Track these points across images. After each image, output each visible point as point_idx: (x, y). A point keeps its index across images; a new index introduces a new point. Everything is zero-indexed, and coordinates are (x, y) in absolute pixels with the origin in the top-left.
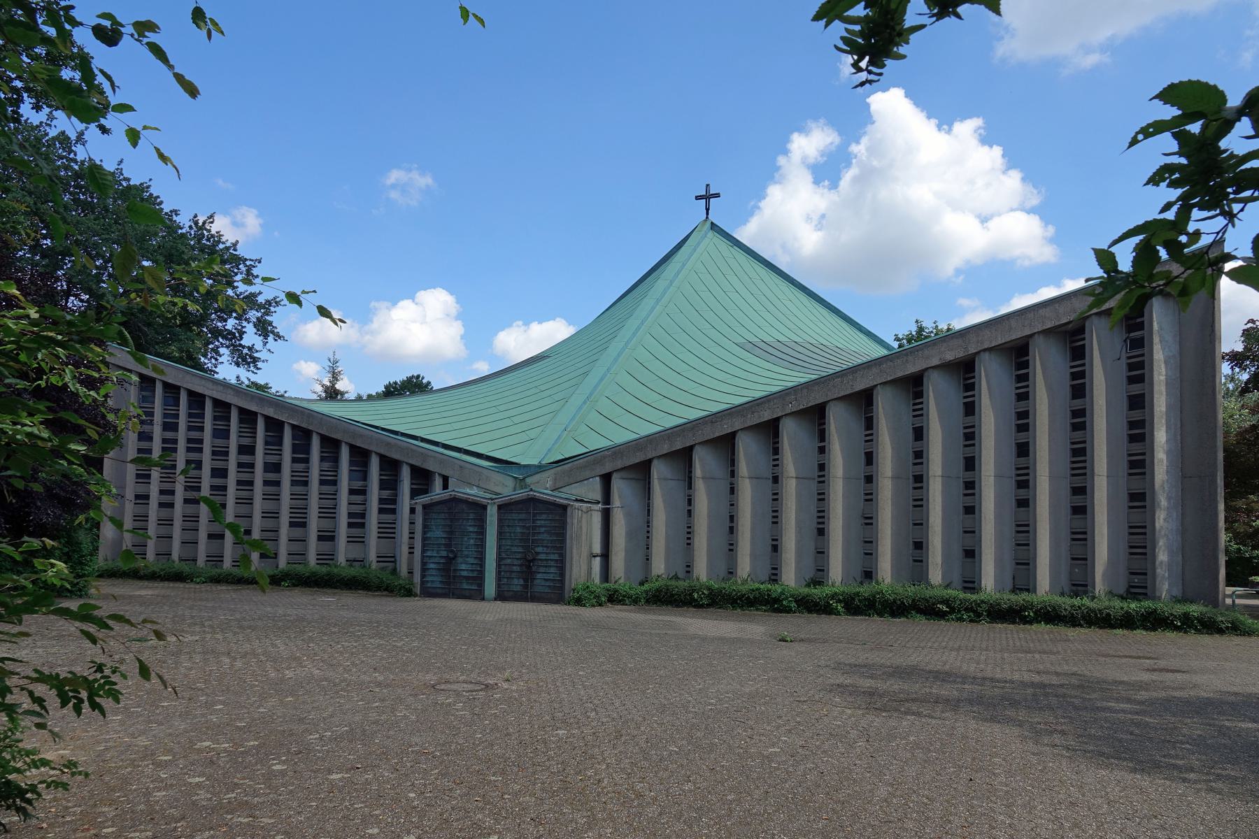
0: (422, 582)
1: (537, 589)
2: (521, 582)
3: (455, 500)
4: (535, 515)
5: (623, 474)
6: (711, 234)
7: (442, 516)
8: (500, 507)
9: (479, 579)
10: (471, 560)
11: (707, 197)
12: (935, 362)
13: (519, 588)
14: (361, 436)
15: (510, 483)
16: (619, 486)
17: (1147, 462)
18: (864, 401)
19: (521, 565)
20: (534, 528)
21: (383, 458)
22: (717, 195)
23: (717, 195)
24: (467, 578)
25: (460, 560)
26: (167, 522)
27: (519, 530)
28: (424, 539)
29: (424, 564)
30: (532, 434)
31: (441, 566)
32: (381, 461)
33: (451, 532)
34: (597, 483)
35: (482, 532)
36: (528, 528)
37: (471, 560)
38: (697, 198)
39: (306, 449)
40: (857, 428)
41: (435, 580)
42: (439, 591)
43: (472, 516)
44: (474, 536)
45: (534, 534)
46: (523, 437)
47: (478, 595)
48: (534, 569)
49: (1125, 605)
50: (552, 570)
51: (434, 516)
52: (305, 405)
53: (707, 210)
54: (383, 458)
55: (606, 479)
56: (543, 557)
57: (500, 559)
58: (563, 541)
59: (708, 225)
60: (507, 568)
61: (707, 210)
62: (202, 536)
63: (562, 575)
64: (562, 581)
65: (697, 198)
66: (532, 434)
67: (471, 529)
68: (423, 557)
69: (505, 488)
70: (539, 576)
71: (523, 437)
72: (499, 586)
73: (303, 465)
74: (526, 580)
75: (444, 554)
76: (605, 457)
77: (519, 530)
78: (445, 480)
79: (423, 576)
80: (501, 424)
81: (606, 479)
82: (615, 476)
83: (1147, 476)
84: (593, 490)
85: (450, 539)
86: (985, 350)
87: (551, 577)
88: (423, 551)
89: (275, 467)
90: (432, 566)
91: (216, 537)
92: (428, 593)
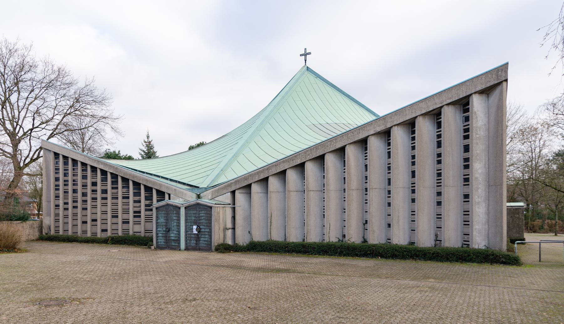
0: (157, 242)
3: (168, 205)
6: (307, 72)
7: (163, 212)
8: (186, 208)
9: (178, 241)
12: (372, 132)
13: (194, 245)
14: (136, 177)
15: (194, 196)
16: (240, 196)
17: (470, 179)
18: (363, 143)
20: (199, 217)
21: (146, 187)
22: (310, 53)
23: (310, 53)
24: (174, 240)
25: (171, 232)
26: (66, 217)
27: (193, 218)
28: (157, 223)
29: (157, 234)
30: (208, 173)
31: (164, 235)
33: (167, 220)
34: (229, 195)
35: (179, 219)
36: (197, 217)
37: (175, 232)
38: (301, 55)
39: (117, 182)
40: (360, 155)
41: (162, 241)
42: (164, 246)
43: (175, 212)
44: (176, 221)
47: (178, 248)
50: (207, 236)
51: (160, 212)
53: (306, 61)
54: (146, 187)
55: (233, 193)
58: (211, 223)
59: (306, 68)
61: (306, 61)
62: (79, 222)
63: (211, 239)
64: (211, 241)
65: (301, 55)
67: (175, 218)
68: (157, 231)
69: (191, 198)
70: (202, 239)
71: (205, 174)
72: (186, 244)
74: (196, 241)
75: (164, 229)
76: (232, 183)
77: (193, 218)
78: (169, 195)
79: (157, 240)
80: (196, 169)
81: (233, 193)
82: (236, 192)
83: (470, 186)
84: (227, 198)
86: (395, 125)
87: (206, 239)
88: (157, 228)
89: (105, 192)
90: (160, 235)
91: (85, 222)
92: (159, 248)
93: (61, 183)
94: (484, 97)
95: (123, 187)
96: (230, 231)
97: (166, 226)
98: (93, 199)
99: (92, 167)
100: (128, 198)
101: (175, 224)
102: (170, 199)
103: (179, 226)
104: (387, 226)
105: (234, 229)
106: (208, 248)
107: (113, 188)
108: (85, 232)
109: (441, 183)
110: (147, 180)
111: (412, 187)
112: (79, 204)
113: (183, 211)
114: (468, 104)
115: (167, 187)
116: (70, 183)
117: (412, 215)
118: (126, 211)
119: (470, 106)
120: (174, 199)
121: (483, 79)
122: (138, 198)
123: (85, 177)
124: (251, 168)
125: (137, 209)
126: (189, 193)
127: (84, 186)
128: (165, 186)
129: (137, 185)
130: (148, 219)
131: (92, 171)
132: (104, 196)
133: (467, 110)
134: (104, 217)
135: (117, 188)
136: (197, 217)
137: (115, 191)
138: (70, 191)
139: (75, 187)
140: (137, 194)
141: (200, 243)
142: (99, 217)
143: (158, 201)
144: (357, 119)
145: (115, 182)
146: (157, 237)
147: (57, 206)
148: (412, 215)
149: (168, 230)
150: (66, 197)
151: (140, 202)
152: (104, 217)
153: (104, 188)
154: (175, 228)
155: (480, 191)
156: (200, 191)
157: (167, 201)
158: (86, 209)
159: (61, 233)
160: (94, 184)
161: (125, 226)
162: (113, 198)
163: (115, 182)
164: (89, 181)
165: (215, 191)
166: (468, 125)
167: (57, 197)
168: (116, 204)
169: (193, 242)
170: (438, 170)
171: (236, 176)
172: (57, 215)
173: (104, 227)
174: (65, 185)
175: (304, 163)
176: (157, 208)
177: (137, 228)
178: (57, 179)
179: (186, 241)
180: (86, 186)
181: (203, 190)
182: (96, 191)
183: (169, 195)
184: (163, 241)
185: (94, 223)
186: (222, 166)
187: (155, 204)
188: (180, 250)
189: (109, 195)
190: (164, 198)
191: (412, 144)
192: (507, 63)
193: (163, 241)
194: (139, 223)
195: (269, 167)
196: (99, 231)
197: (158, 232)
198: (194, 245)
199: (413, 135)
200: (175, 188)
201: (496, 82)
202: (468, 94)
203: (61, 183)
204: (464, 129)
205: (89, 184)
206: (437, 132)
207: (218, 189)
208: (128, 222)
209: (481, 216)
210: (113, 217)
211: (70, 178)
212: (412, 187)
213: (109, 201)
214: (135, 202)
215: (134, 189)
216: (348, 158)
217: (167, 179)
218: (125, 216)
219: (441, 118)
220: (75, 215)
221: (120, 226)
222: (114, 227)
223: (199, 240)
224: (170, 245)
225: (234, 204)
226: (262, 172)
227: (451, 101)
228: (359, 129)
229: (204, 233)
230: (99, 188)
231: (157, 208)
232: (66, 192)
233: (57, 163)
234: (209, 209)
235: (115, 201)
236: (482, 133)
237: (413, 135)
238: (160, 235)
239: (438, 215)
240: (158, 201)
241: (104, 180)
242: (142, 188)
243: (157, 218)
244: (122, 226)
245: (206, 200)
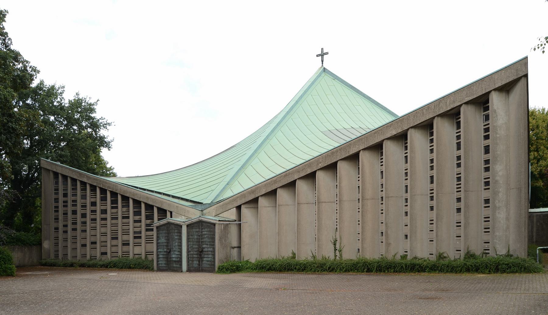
0: (158, 264)
1: (204, 265)
2: (197, 262)
3: (169, 224)
4: (202, 229)
5: (246, 206)
8: (188, 226)
9: (180, 262)
10: (177, 253)
11: (322, 55)
13: (196, 266)
19: (197, 254)
20: (202, 235)
22: (327, 53)
23: (327, 53)
25: (172, 253)
26: (66, 240)
28: (158, 243)
29: (158, 255)
30: (213, 188)
31: (165, 256)
32: (133, 202)
33: (168, 240)
35: (180, 239)
36: (199, 236)
37: (177, 253)
38: (317, 56)
41: (163, 263)
42: (165, 268)
43: (176, 231)
44: (177, 241)
45: (202, 238)
46: (209, 189)
47: (179, 270)
48: (203, 256)
49: (18, 234)
50: (210, 256)
51: (161, 232)
52: (125, 182)
53: (322, 61)
55: (239, 208)
56: (206, 250)
57: (188, 252)
60: (191, 256)
61: (322, 61)
62: (79, 245)
65: (317, 56)
66: (213, 188)
67: (176, 237)
68: (157, 252)
69: (195, 215)
70: (205, 259)
71: (209, 189)
72: (188, 265)
73: (116, 210)
74: (199, 261)
75: (165, 250)
79: (158, 261)
81: (239, 208)
84: (231, 215)
85: (168, 243)
87: (209, 259)
88: (157, 249)
89: (104, 212)
90: (161, 256)
92: (160, 270)
93: (61, 204)
94: (503, 95)
95: (123, 207)
96: (236, 249)
97: (167, 246)
98: (92, 220)
99: (91, 186)
100: (128, 217)
101: (177, 244)
102: (171, 217)
103: (180, 246)
104: (404, 237)
105: (239, 247)
106: (211, 269)
107: (112, 208)
108: (84, 256)
109: (460, 188)
110: (147, 198)
111: (431, 193)
112: (79, 227)
113: (184, 230)
114: (487, 101)
115: (169, 205)
116: (70, 203)
117: (431, 224)
118: (126, 232)
119: (490, 104)
120: (176, 217)
121: (503, 74)
122: (138, 217)
123: (84, 197)
124: (258, 180)
125: (137, 230)
126: (192, 210)
127: (84, 206)
128: (166, 203)
129: (137, 203)
130: (149, 240)
131: (91, 190)
132: (103, 216)
133: (487, 109)
134: (103, 239)
135: (117, 207)
136: (199, 236)
137: (114, 211)
138: (70, 213)
139: (65, 199)
140: (137, 213)
141: (201, 263)
142: (98, 239)
143: (159, 219)
144: (374, 121)
145: (114, 202)
146: (158, 258)
147: (57, 229)
148: (431, 224)
149: (169, 253)
150: (66, 219)
151: (140, 221)
152: (103, 239)
153: (103, 208)
154: (176, 248)
155: (500, 195)
156: (203, 207)
157: (168, 219)
158: (85, 231)
159: (69, 257)
160: (94, 204)
161: (125, 248)
162: (112, 219)
163: (114, 202)
164: (88, 201)
165: (220, 206)
166: (489, 124)
167: (57, 219)
168: (116, 225)
169: (196, 263)
170: (458, 174)
171: (253, 185)
172: (57, 238)
173: (103, 250)
174: (64, 206)
175: (295, 181)
176: (157, 227)
177: (137, 250)
178: (56, 200)
179: (188, 262)
180: (85, 206)
181: (207, 206)
182: (95, 211)
183: (171, 213)
184: (164, 262)
185: (93, 246)
186: (228, 179)
187: (157, 222)
188: (182, 272)
189: (108, 216)
190: (166, 216)
191: (431, 146)
192: (526, 58)
193: (164, 262)
194: (139, 245)
195: (297, 169)
196: (98, 255)
197: (159, 253)
198: (196, 266)
199: (432, 138)
200: (177, 205)
201: (515, 77)
202: (487, 91)
203: (61, 204)
204: (484, 129)
205: (88, 205)
206: (457, 133)
207: (221, 204)
208: (128, 244)
209: (502, 222)
210: (113, 238)
211: (70, 198)
212: (431, 193)
213: (109, 222)
214: (135, 221)
215: (134, 208)
216: (363, 165)
217: (169, 195)
218: (125, 238)
219: (460, 118)
220: (75, 237)
221: (120, 249)
222: (114, 249)
223: (202, 261)
224: (171, 265)
225: (240, 221)
226: (275, 182)
227: (471, 98)
228: (375, 133)
229: (207, 253)
230: (98, 208)
231: (157, 227)
232: (65, 214)
233: (57, 183)
234: (212, 226)
235: (114, 221)
236: (503, 133)
237: (432, 138)
238: (161, 256)
239: (457, 223)
240: (159, 219)
241: (104, 199)
242: (143, 206)
243: (158, 238)
244: (122, 248)
245: (210, 217)
